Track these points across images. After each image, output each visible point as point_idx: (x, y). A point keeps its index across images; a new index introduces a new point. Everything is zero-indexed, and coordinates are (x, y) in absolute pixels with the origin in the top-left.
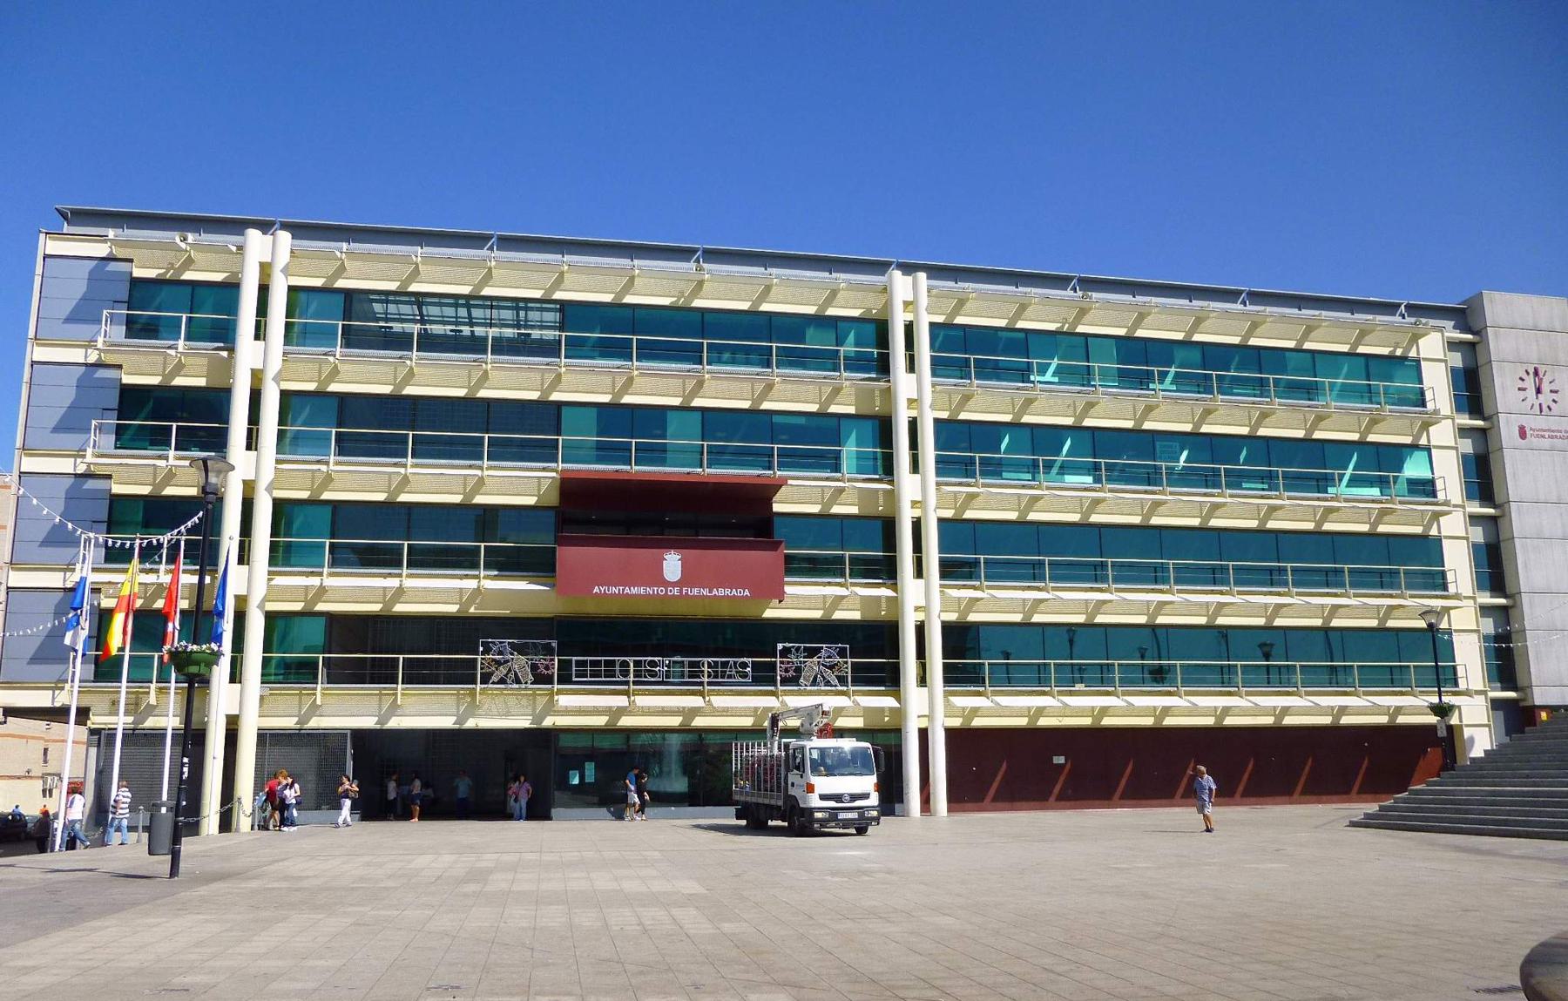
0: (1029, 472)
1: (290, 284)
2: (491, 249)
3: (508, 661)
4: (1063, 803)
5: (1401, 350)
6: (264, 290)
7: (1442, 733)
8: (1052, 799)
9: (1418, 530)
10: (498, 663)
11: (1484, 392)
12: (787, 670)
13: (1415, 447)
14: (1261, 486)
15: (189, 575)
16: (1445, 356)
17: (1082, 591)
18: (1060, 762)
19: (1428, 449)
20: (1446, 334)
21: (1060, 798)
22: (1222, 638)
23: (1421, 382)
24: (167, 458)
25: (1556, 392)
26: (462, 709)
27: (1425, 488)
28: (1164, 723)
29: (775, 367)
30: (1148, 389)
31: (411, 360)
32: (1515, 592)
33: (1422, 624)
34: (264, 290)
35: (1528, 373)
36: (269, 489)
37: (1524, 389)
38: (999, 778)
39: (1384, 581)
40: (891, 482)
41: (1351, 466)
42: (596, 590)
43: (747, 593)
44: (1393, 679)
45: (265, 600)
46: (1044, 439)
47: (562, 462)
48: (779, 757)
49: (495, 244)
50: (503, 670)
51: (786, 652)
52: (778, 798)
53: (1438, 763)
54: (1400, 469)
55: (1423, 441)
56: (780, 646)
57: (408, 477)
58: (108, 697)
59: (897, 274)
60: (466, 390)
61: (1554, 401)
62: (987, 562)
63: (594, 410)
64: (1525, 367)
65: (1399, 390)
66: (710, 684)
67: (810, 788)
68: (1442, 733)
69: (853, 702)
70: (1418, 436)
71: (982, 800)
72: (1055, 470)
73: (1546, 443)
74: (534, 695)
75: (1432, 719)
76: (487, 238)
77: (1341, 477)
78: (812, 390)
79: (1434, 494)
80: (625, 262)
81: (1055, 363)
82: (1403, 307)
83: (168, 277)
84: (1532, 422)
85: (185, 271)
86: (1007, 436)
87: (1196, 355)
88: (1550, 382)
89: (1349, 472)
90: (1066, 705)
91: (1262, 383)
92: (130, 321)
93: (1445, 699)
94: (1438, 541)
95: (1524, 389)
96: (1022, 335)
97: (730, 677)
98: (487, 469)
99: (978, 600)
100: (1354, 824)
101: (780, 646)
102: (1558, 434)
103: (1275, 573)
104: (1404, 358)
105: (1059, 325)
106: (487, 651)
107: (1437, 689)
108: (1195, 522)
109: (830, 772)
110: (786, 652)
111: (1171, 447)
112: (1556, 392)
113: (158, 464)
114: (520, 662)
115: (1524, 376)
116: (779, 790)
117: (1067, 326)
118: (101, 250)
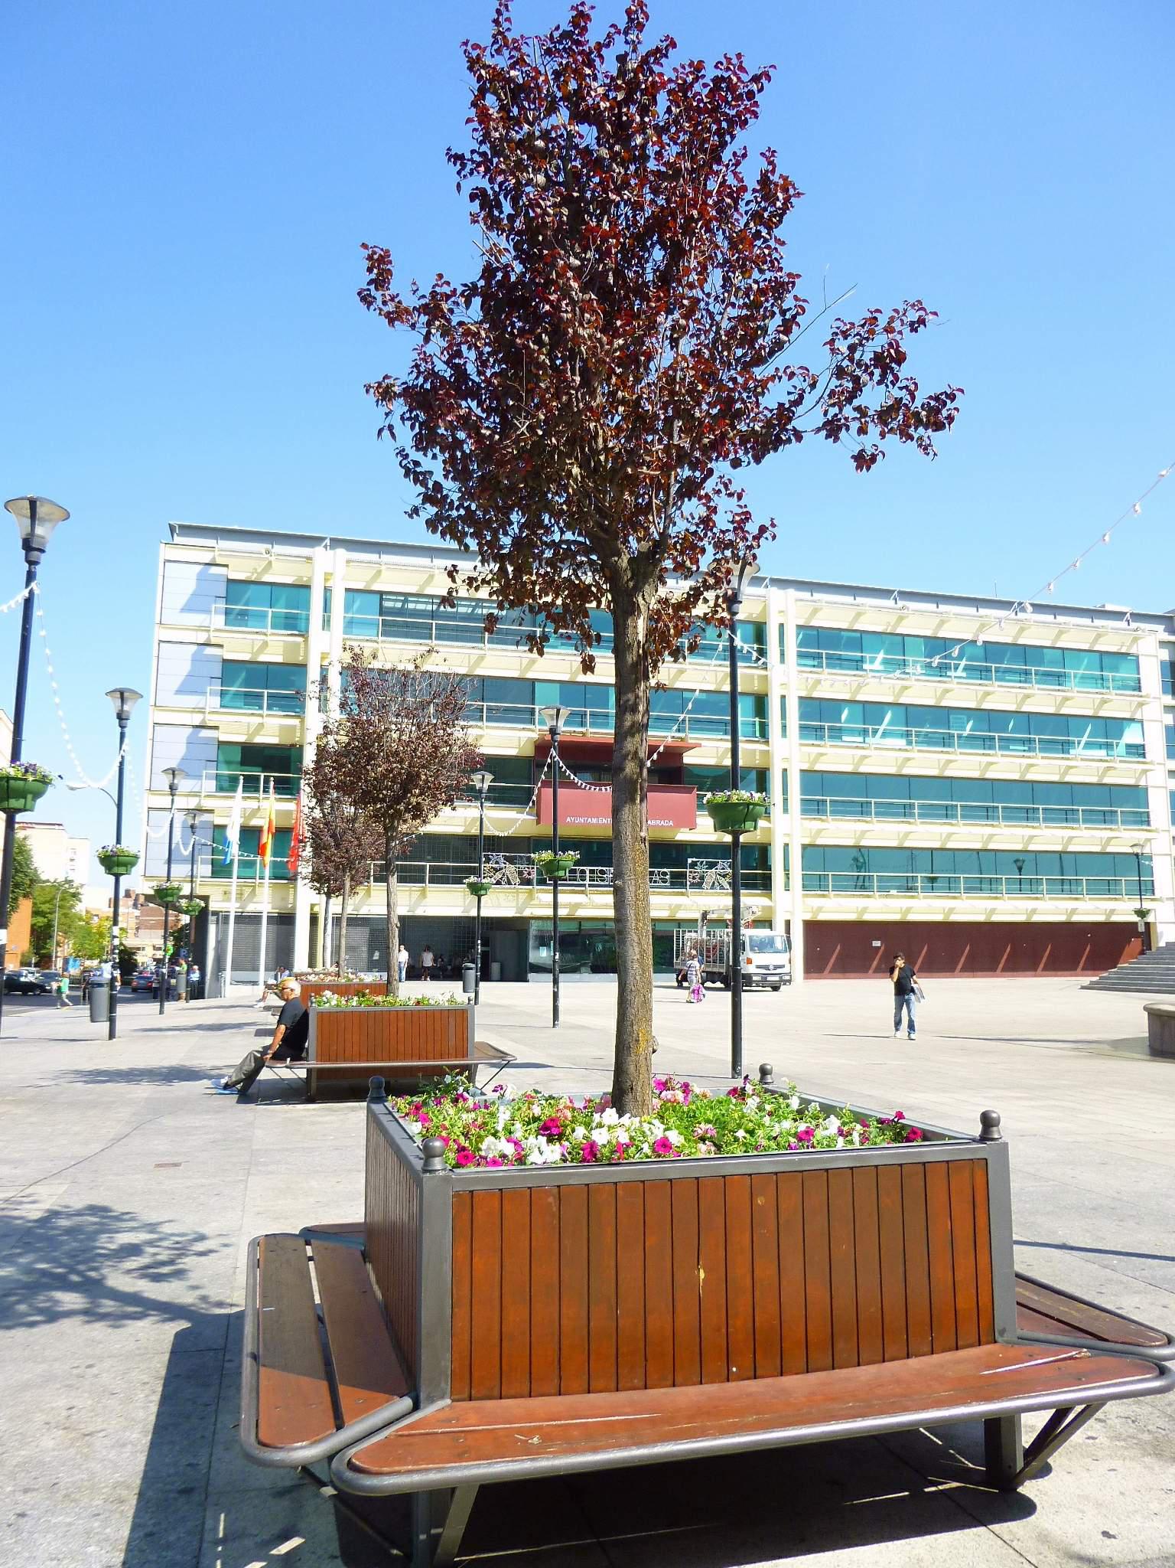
2: (767, 587)
3: (501, 869)
7: (1141, 929)
8: (871, 971)
10: (496, 870)
12: (694, 878)
13: (1132, 720)
14: (1022, 748)
19: (1141, 722)
22: (910, 856)
26: (413, 900)
27: (1138, 751)
30: (946, 676)
38: (834, 956)
39: (1107, 818)
40: (767, 742)
42: (568, 819)
43: (671, 823)
44: (1109, 888)
46: (871, 712)
48: (702, 941)
50: (498, 875)
51: (694, 865)
52: (722, 967)
53: (1139, 948)
54: (1120, 736)
55: (1138, 716)
56: (690, 861)
58: (223, 889)
63: (558, 685)
65: (1123, 679)
66: (590, 886)
67: (749, 961)
68: (1141, 929)
70: (1134, 712)
74: (517, 893)
75: (1135, 918)
77: (1079, 743)
79: (1144, 755)
80: (374, 557)
81: (881, 656)
89: (1084, 739)
91: (1027, 673)
92: (227, 612)
97: (655, 882)
100: (1083, 988)
101: (690, 861)
103: (1030, 811)
106: (488, 860)
109: (761, 951)
110: (694, 865)
114: (511, 869)
116: (721, 961)
118: (207, 557)
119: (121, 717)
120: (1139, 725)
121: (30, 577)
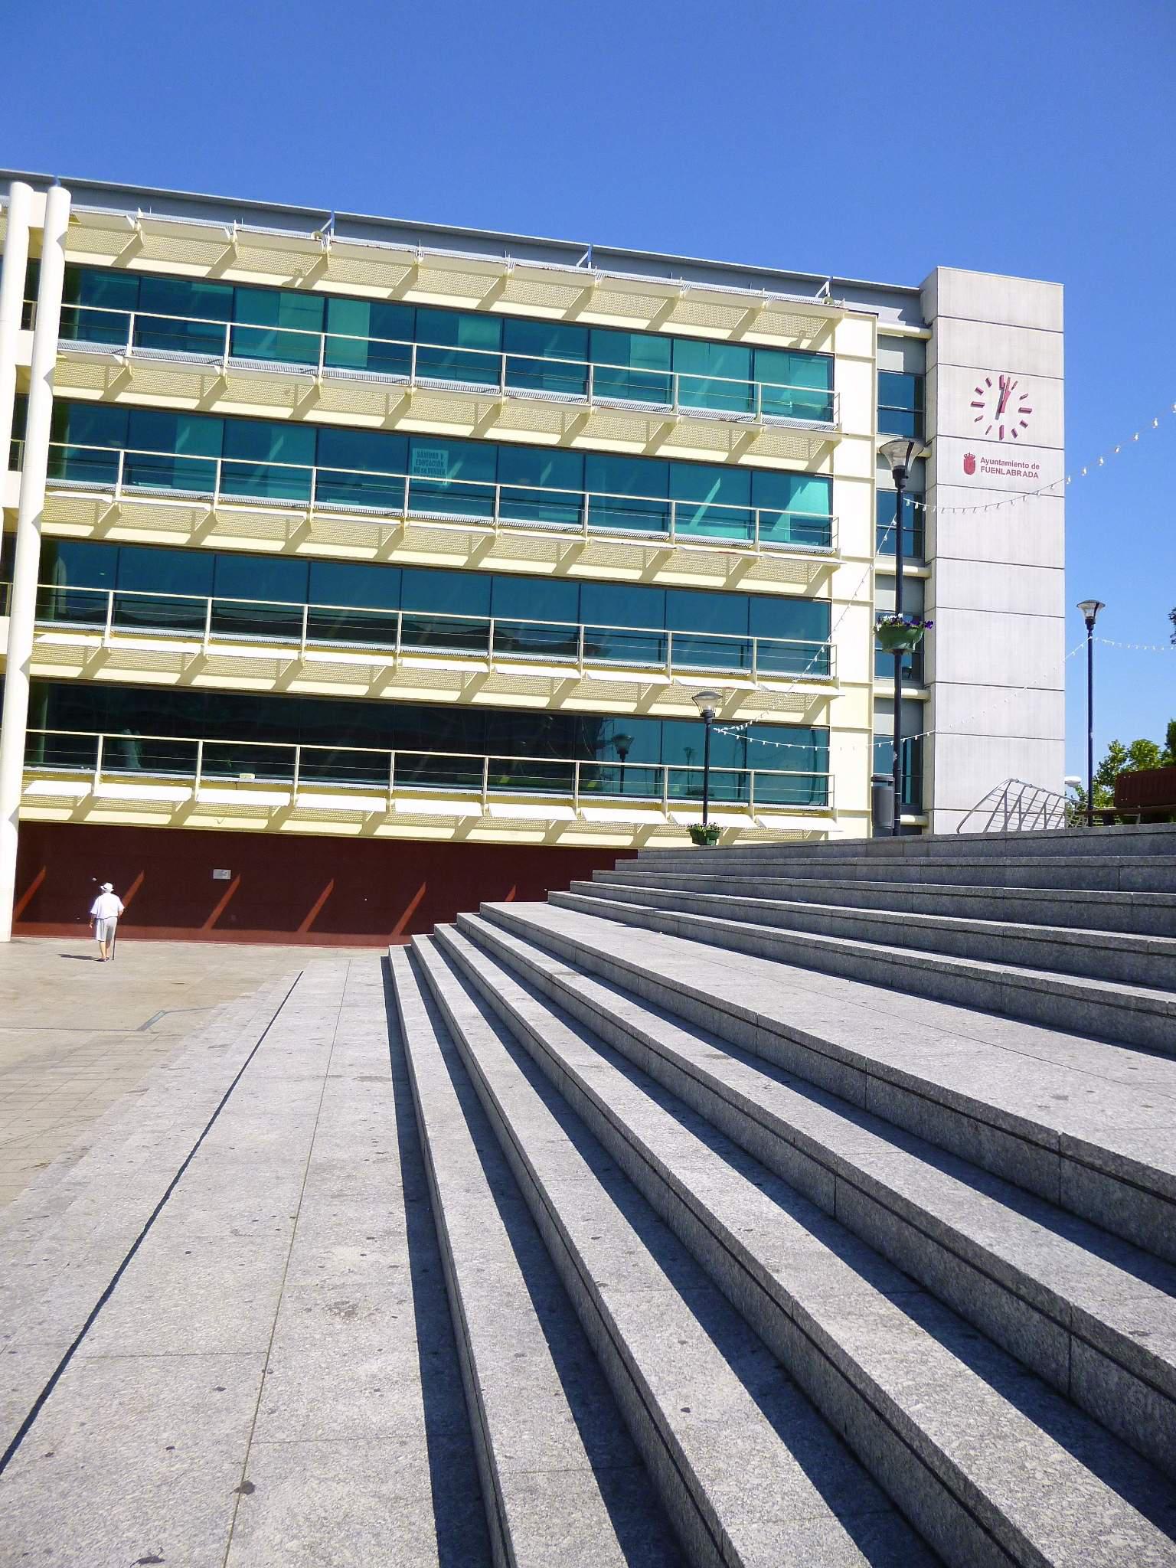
0: (745, 527)
1: (68, 260)
4: (222, 931)
5: (809, 341)
6: (34, 268)
9: (799, 589)
11: (929, 407)
15: (83, 636)
16: (874, 354)
17: (549, 665)
18: (224, 877)
19: (828, 479)
20: (879, 325)
21: (218, 925)
23: (831, 386)
24: (113, 493)
25: (1028, 411)
28: (468, 838)
29: (677, 403)
31: (222, 366)
32: (930, 681)
33: (695, 712)
34: (34, 268)
35: (988, 382)
36: (37, 522)
37: (981, 405)
41: (712, 495)
45: (30, 661)
47: (316, 500)
49: (333, 226)
54: (784, 503)
55: (824, 469)
57: (310, 524)
59: (20, 189)
60: (102, 392)
61: (1023, 424)
62: (588, 632)
64: (987, 374)
69: (668, 819)
71: (200, 926)
72: (696, 520)
73: (1004, 480)
76: (579, 251)
78: (720, 433)
82: (827, 285)
83: (296, 286)
84: (980, 451)
85: (318, 280)
86: (719, 480)
87: (493, 332)
88: (1021, 398)
90: (762, 826)
93: (713, 818)
94: (826, 606)
95: (981, 405)
96: (230, 290)
98: (314, 511)
99: (664, 687)
102: (1023, 470)
104: (809, 354)
105: (288, 279)
107: (702, 802)
108: (548, 568)
111: (435, 455)
112: (1028, 411)
113: (104, 499)
115: (984, 386)
117: (300, 280)
119: (1090, 622)
120: (825, 486)
121: (1090, 634)
